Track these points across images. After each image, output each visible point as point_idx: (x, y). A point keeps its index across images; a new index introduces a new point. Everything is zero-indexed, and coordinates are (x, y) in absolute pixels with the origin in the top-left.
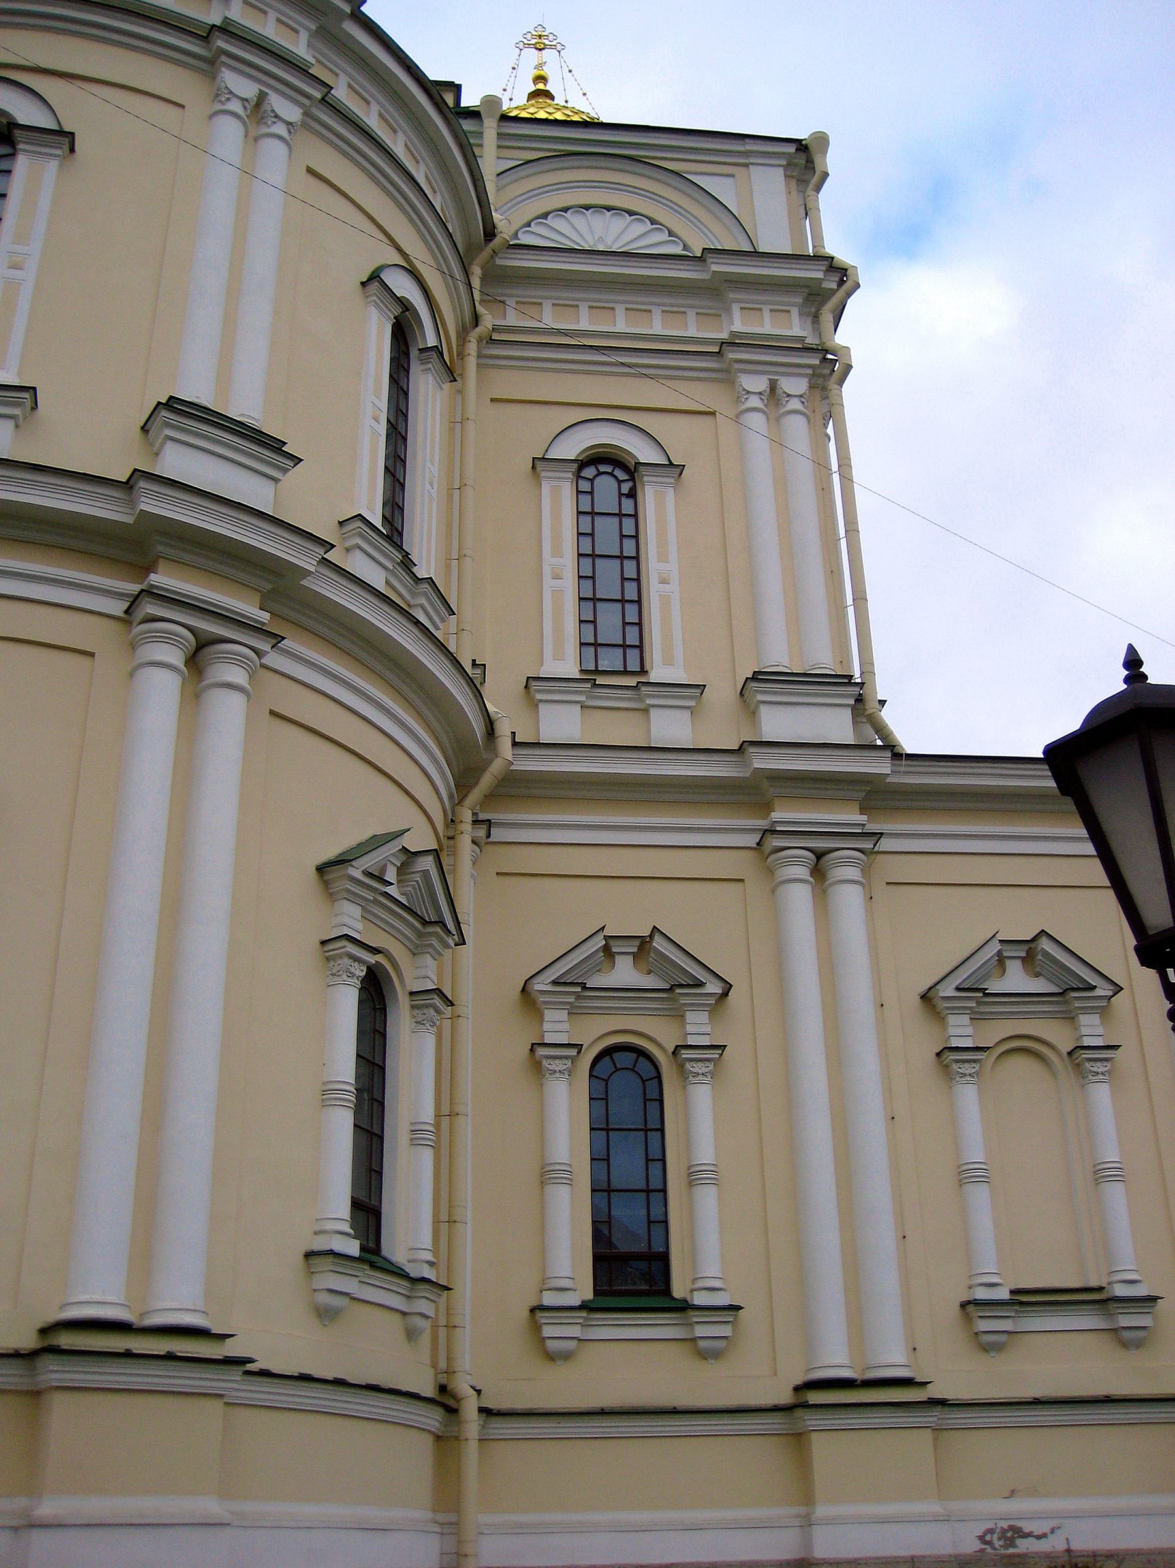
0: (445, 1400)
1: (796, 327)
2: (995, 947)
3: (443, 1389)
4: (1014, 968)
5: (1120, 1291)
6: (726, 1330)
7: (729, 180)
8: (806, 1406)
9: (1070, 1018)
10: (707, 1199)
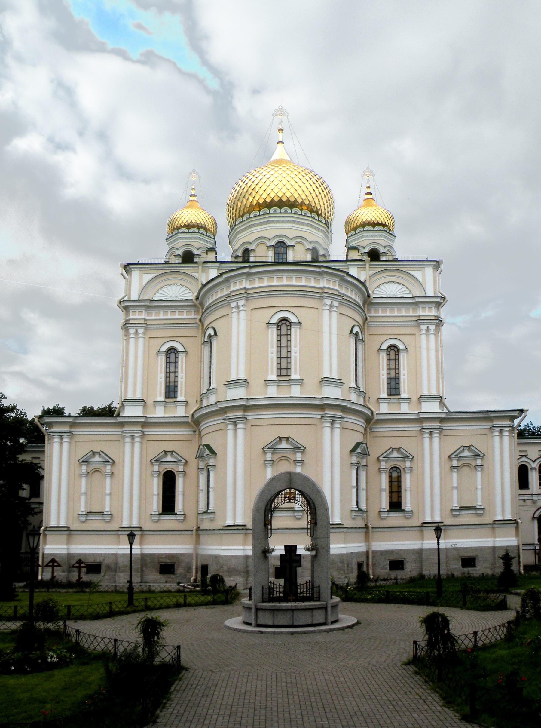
0: (366, 527)
1: (434, 312)
2: (462, 448)
3: (366, 525)
4: (466, 451)
5: (478, 507)
6: (482, 512)
7: (421, 272)
8: (423, 526)
9: (405, 462)
10: (408, 494)
